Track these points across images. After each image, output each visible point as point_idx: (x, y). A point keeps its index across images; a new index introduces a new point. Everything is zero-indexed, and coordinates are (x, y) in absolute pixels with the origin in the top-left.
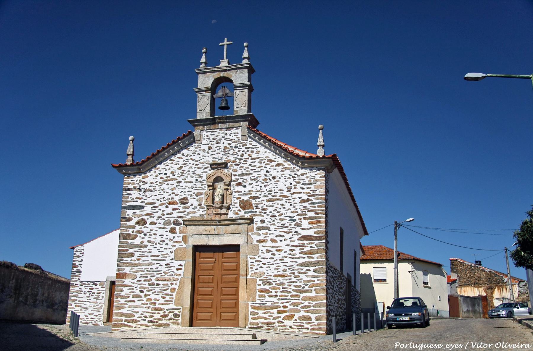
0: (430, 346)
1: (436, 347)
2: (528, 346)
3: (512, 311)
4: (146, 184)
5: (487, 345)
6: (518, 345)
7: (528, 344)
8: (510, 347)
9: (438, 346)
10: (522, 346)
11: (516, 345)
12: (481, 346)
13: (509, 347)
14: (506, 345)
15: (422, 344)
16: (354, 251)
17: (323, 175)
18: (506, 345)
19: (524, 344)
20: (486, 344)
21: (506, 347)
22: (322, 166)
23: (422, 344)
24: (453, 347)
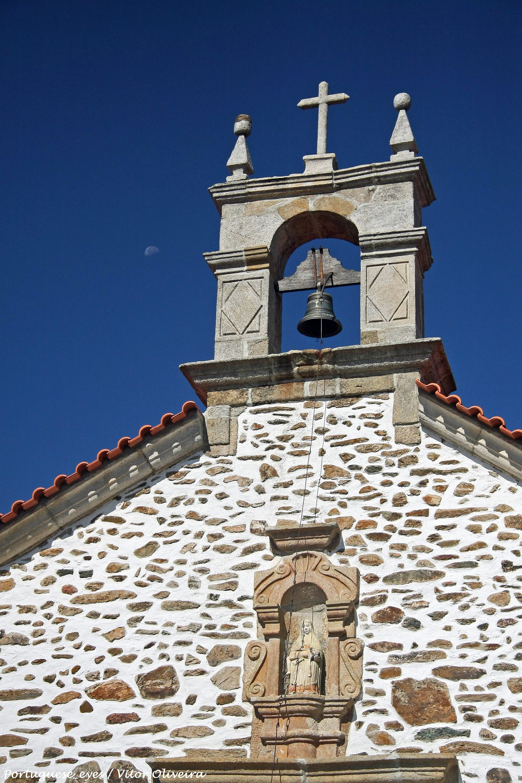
4: (279, 509)
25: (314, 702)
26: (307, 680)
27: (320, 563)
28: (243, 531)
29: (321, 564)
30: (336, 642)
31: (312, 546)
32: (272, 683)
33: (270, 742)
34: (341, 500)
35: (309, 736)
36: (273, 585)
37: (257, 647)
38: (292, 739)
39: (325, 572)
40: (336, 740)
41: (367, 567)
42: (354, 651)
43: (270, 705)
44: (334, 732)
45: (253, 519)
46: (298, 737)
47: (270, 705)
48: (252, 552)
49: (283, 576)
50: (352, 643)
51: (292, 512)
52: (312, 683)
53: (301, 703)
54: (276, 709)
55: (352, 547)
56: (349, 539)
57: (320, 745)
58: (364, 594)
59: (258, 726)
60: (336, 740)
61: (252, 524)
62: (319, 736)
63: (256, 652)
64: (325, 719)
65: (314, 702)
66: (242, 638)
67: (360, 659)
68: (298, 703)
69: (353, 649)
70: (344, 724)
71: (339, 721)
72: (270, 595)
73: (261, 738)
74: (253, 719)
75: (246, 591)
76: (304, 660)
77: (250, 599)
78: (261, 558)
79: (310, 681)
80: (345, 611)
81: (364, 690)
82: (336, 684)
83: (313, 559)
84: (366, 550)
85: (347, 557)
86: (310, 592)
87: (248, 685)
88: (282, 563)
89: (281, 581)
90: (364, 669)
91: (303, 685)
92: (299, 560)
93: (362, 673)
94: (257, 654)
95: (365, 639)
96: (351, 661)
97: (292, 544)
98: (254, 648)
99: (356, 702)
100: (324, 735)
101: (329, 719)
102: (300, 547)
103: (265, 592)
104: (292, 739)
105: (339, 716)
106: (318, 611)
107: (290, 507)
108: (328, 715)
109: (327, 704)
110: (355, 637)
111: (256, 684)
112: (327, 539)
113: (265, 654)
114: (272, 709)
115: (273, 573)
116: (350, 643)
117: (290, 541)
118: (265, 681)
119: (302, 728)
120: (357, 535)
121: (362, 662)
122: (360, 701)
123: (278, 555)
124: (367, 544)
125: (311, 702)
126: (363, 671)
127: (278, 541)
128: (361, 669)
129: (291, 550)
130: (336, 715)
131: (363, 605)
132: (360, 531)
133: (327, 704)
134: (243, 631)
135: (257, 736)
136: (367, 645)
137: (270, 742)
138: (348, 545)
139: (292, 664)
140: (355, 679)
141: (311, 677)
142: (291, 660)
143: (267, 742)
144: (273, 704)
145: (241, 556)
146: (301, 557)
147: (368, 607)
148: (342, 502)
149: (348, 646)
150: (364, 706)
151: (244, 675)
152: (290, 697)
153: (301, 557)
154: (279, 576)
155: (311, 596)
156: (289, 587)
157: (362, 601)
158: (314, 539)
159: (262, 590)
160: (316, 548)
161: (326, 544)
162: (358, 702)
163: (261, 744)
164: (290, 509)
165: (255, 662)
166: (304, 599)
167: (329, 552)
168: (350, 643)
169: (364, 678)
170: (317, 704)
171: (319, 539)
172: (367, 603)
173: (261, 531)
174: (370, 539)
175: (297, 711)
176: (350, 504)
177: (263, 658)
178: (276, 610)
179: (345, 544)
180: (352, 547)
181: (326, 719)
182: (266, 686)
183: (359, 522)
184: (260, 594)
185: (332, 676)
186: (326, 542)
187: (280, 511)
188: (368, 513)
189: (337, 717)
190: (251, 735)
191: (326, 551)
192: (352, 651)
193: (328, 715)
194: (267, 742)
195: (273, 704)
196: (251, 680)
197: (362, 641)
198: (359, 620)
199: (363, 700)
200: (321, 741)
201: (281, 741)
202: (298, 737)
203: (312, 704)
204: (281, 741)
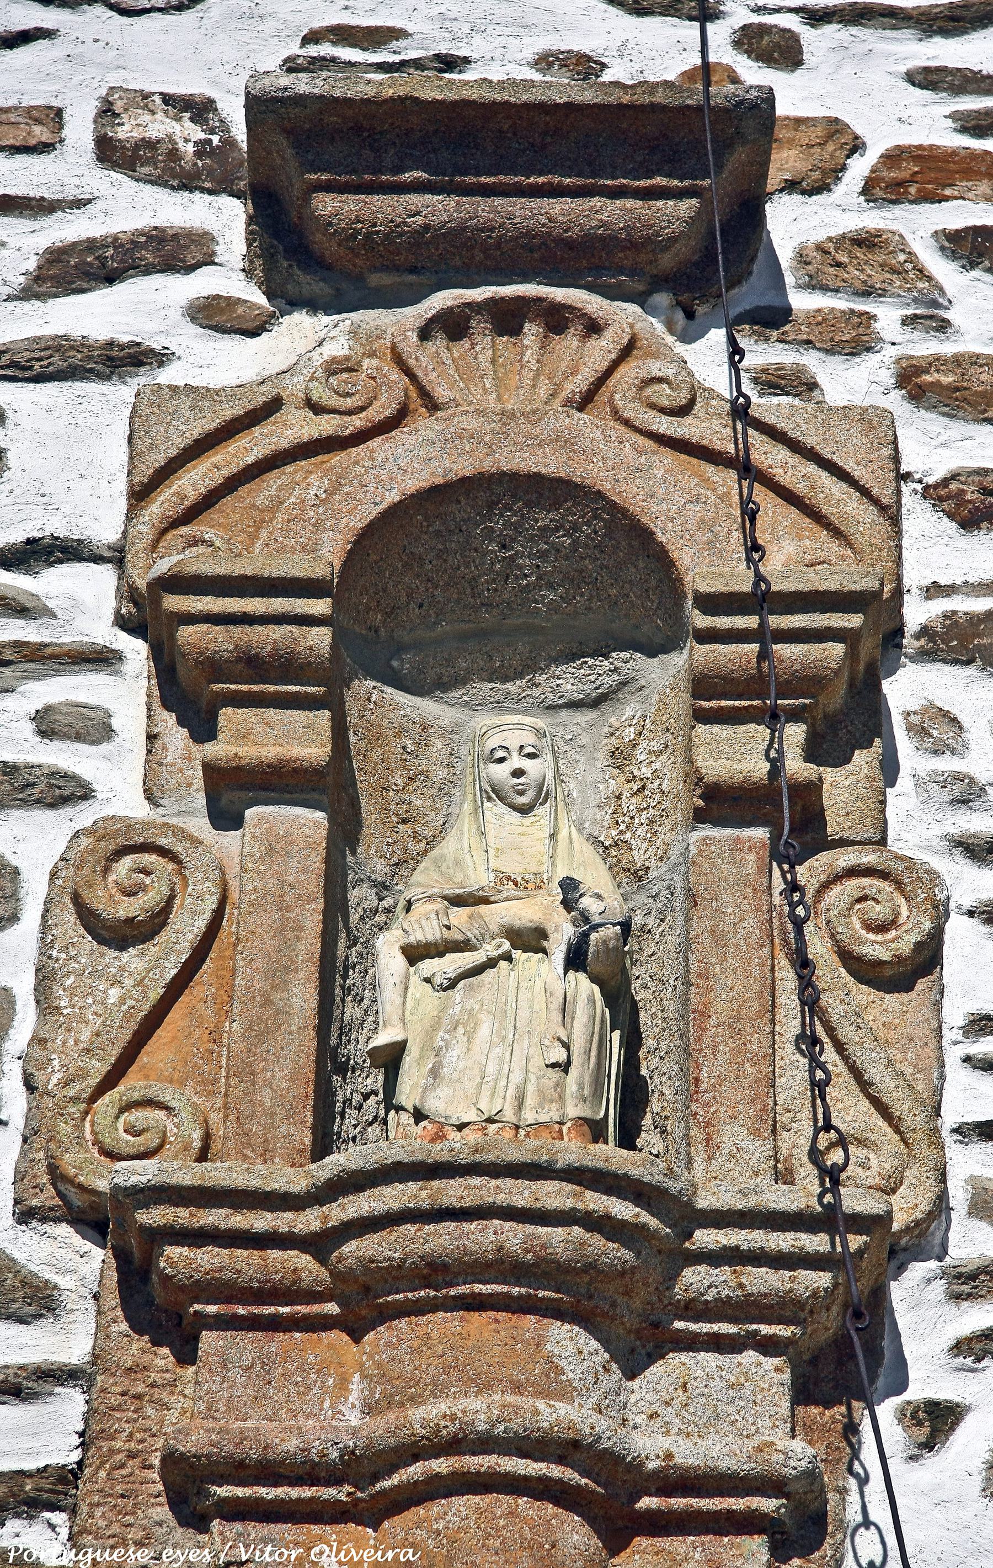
0: (115, 1556)
1: (133, 1557)
2: (410, 1555)
3: (181, 1312)
4: (312, 38)
5: (286, 1553)
6: (380, 1553)
7: (411, 1551)
8: (356, 1559)
9: (139, 1554)
10: (390, 1555)
11: (373, 1551)
12: (267, 1554)
13: (352, 1558)
14: (343, 1553)
15: (90, 1550)
16: (27, 306)
17: (776, 872)
18: (343, 1553)
19: (398, 1550)
20: (283, 1550)
21: (412, 1559)
22: (716, 1258)
23: (90, 1550)
24: (182, 1559)
25: (623, 1210)
26: (541, 1093)
27: (622, 370)
28: (44, 148)
29: (629, 372)
30: (752, 857)
31: (570, 244)
32: (266, 1096)
33: (240, 1492)
34: (756, 19)
35: (575, 1444)
36: (273, 482)
37: (149, 859)
38: (441, 1465)
39: (664, 425)
40: (767, 1504)
41: (958, 429)
42: (882, 928)
43: (261, 1221)
44: (751, 1444)
45: (114, 79)
46: (486, 1444)
47: (261, 1221)
48: (111, 279)
49: (357, 422)
50: (869, 872)
51: (403, 63)
52: (573, 1110)
53: (520, 1202)
54: (303, 1261)
55: (840, 303)
56: (820, 248)
57: (641, 1542)
58: (934, 590)
59: (141, 1388)
60: (767, 1504)
61: (107, 112)
62: (636, 1466)
63: (142, 888)
64: (678, 1360)
65: (623, 1210)
66: (26, 803)
67: (921, 985)
68: (501, 1199)
69: (878, 911)
70: (814, 1410)
71: (786, 1376)
72: (254, 537)
73: (171, 1460)
74: (101, 1330)
75: (66, 509)
76: (508, 957)
77: (97, 559)
78: (176, 314)
79: (561, 1098)
80: (837, 650)
81: (959, 1196)
82: (755, 1133)
83: (570, 341)
84: (943, 326)
85: (812, 361)
86: (543, 555)
87: (75, 1100)
88: (338, 348)
89: (337, 459)
90: (953, 1056)
91: (509, 1115)
92: (466, 343)
93: (942, 1077)
94: (149, 899)
95: (956, 868)
96: (864, 994)
97: (435, 221)
98: (127, 862)
99: (902, 1268)
100: (678, 1460)
101: (710, 1360)
102: (485, 248)
103: (213, 514)
104: (441, 1465)
105: (790, 1342)
106: (574, 705)
107: (395, 34)
108: (705, 1327)
109: (706, 1238)
110: (883, 842)
111: (136, 1096)
112: (687, 207)
113: (211, 903)
114: (274, 1254)
115: (274, 406)
116: (853, 872)
117: (415, 200)
118: (208, 1086)
119: (518, 1388)
120: (878, 234)
121: (938, 1005)
122: (933, 1264)
123: (314, 306)
124: (950, 291)
125: (595, 1202)
126: (948, 1070)
127: (328, 188)
128: (930, 1051)
129: (413, 270)
130: (765, 1329)
131: (925, 656)
132: (898, 210)
133: (706, 1238)
134: (33, 759)
135: (132, 1455)
136: (967, 903)
137: (240, 1492)
138: (814, 284)
139: (414, 980)
140: (902, 1106)
141: (565, 1067)
142: (414, 954)
143: (223, 1491)
144: (283, 1221)
145: (26, 294)
146: (478, 324)
147: (971, 671)
148: (763, 30)
149: (836, 889)
150: (957, 1297)
151: (38, 1040)
152: (445, 1157)
153: (478, 324)
154: (326, 426)
155: (537, 586)
156: (393, 497)
157: (925, 631)
158: (597, 202)
159: (192, 496)
160: (598, 269)
161: (673, 240)
162: (918, 1270)
163: (163, 1512)
164: (394, 44)
165: (132, 959)
166: (488, 605)
167: (680, 316)
168: (853, 872)
169: (951, 1116)
170: (644, 1227)
171: (630, 203)
172: (963, 645)
173: (174, 154)
174: (972, 265)
175: (488, 1265)
176: (827, 44)
177: (201, 924)
178: (320, 606)
179: (789, 280)
180: (840, 303)
181: (684, 1357)
182: (215, 1118)
183: (893, 157)
184: (175, 523)
185: (721, 1079)
186: (677, 227)
187: (314, 50)
188: (948, 110)
189: (768, 1346)
190: (76, 1456)
191: (662, 299)
192: (869, 927)
193: (705, 1327)
194: (223, 1491)
195: (283, 1221)
196: (99, 1068)
197: (934, 875)
198: (904, 744)
199: (948, 1260)
200: (647, 1502)
201: (329, 1493)
202: (486, 1444)
203: (608, 1217)
204: (329, 1493)
